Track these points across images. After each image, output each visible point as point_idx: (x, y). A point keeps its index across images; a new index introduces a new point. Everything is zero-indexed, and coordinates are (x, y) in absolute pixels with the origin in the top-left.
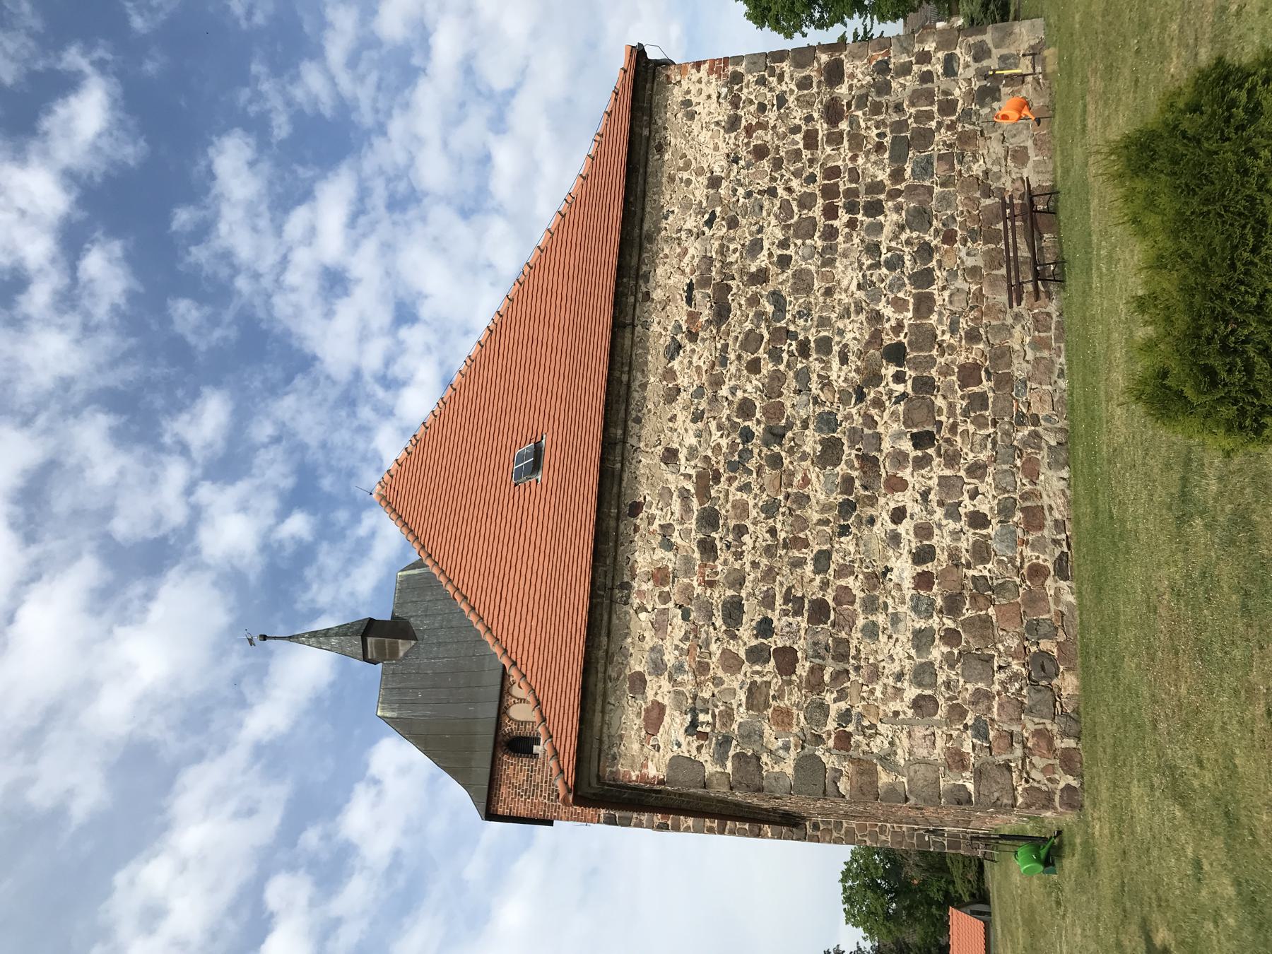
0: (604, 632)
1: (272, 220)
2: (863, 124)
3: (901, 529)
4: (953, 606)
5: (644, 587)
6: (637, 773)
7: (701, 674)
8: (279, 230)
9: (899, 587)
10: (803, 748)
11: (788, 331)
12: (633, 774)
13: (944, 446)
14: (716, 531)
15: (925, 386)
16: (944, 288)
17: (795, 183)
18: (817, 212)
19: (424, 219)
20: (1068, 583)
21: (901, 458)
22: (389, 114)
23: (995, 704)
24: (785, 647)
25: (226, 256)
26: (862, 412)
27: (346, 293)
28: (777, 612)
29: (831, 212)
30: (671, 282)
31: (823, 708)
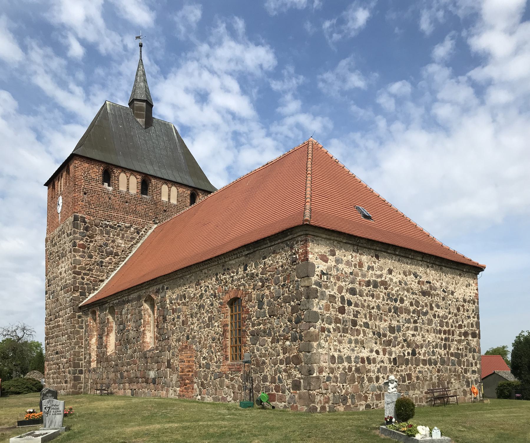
1: (234, 71)
2: (463, 344)
3: (374, 353)
4: (358, 370)
6: (310, 250)
7: (337, 278)
8: (230, 74)
9: (361, 352)
10: (320, 315)
11: (419, 316)
12: (309, 248)
15: (407, 362)
16: (428, 369)
17: (451, 321)
18: (445, 328)
19: (228, 148)
20: (365, 408)
22: (275, 139)
23: (335, 384)
25: (220, 43)
26: (401, 341)
27: (197, 102)
28: (353, 308)
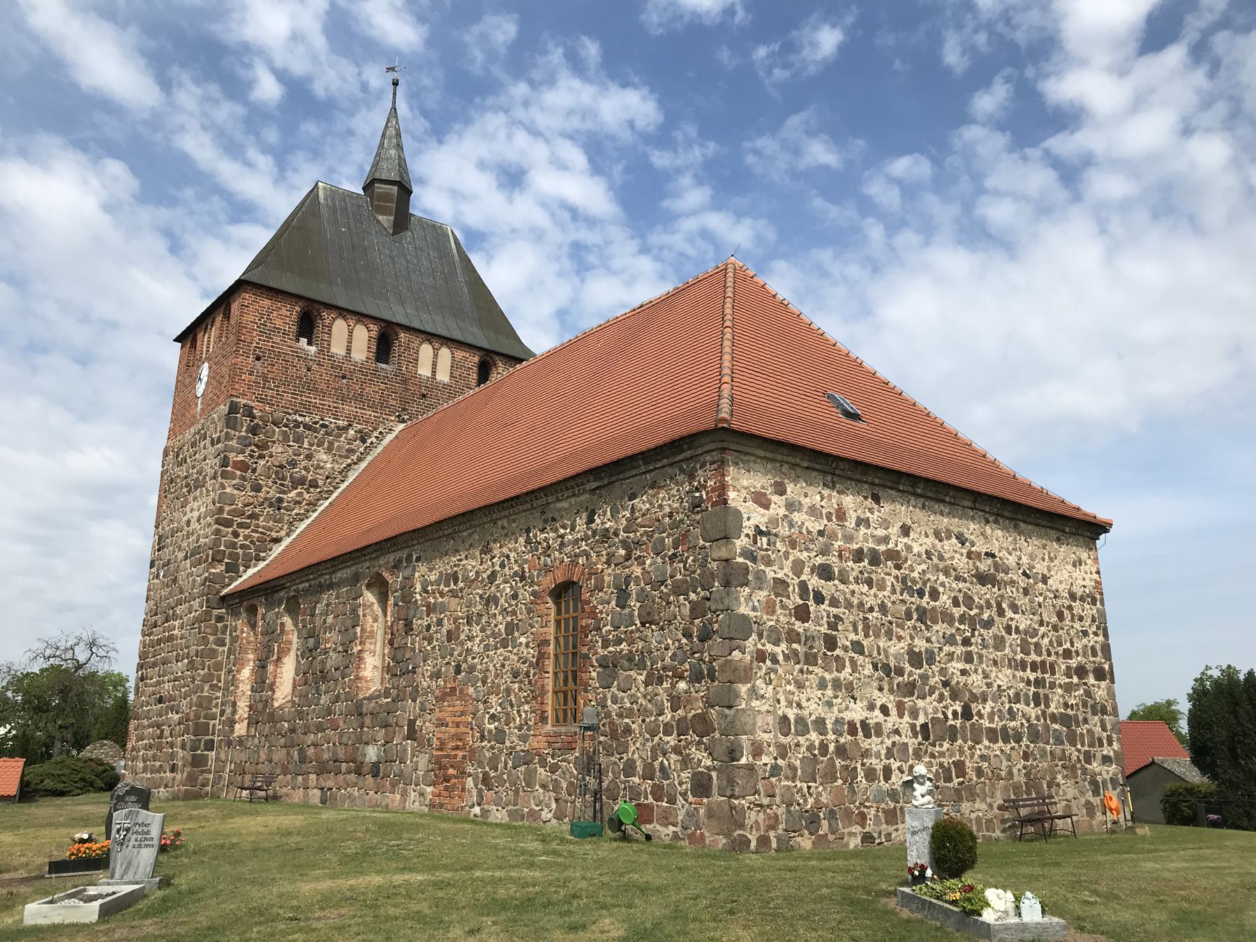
0: (810, 464)
1: (578, 131)
3: (877, 712)
4: (841, 751)
5: (834, 501)
7: (790, 542)
8: (571, 136)
9: (847, 708)
10: (755, 622)
12: (729, 478)
13: (923, 748)
14: (869, 564)
15: (953, 734)
16: (1002, 751)
17: (1046, 640)
19: (560, 274)
21: (915, 714)
22: (657, 259)
23: (790, 783)
24: (809, 613)
26: (937, 685)
27: (501, 186)
28: (828, 608)
29: (1034, 667)
30: (994, 541)
31: (776, 643)
